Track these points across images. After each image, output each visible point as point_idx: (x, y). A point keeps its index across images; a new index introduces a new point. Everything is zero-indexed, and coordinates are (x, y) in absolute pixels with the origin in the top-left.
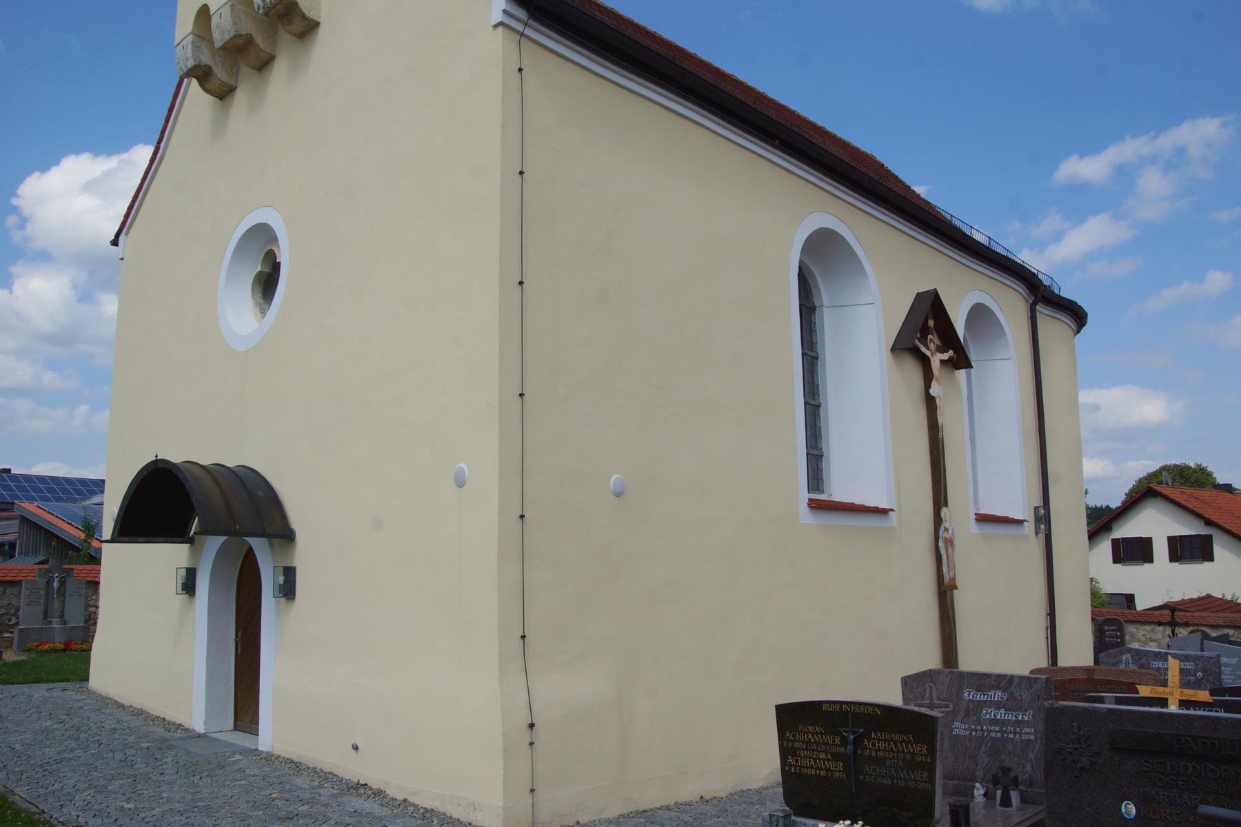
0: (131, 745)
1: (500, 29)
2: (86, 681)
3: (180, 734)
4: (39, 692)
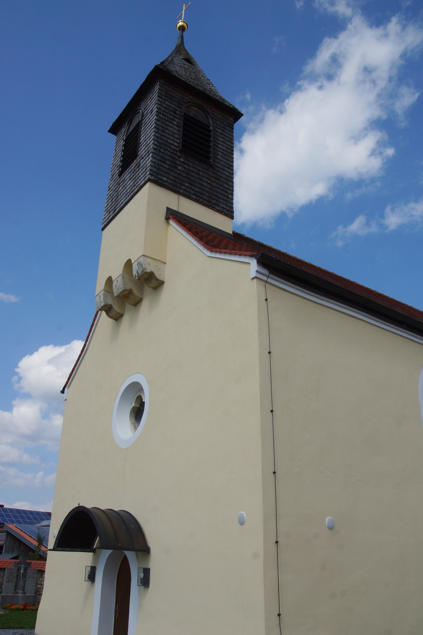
1: (255, 280)
2: (32, 629)
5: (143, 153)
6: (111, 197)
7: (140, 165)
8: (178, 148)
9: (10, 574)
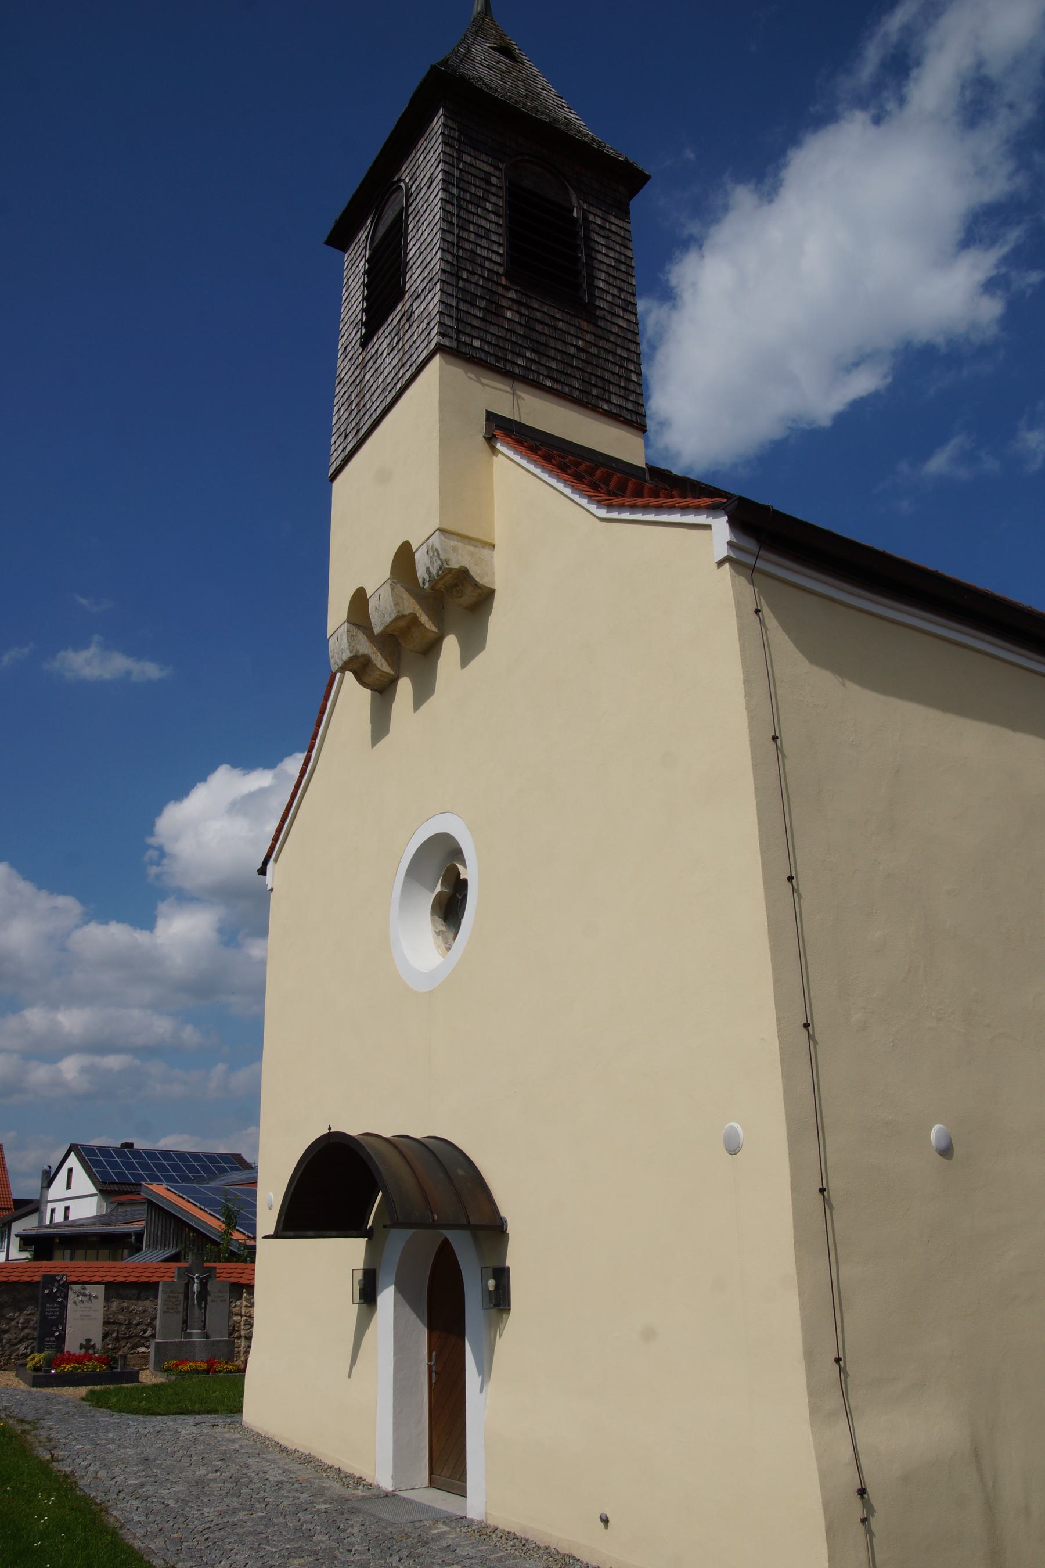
0: (305, 1506)
2: (236, 1412)
3: (363, 1491)
4: (186, 1427)
5: (419, 286)
6: (347, 399)
7: (413, 315)
8: (503, 268)
9: (171, 1295)
